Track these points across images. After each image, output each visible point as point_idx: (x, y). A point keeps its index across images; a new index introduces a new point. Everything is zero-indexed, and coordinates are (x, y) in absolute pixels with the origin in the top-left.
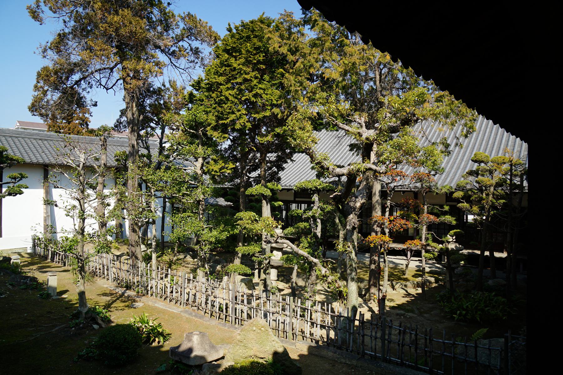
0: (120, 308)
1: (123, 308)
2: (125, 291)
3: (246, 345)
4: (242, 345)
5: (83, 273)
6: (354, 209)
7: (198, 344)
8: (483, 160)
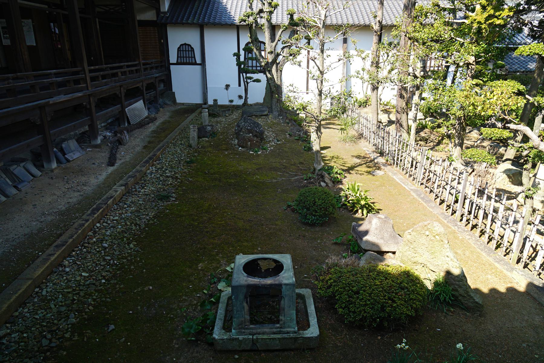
0: (360, 172)
1: (363, 173)
2: (378, 157)
3: (416, 249)
4: (412, 247)
5: (319, 133)
7: (376, 229)
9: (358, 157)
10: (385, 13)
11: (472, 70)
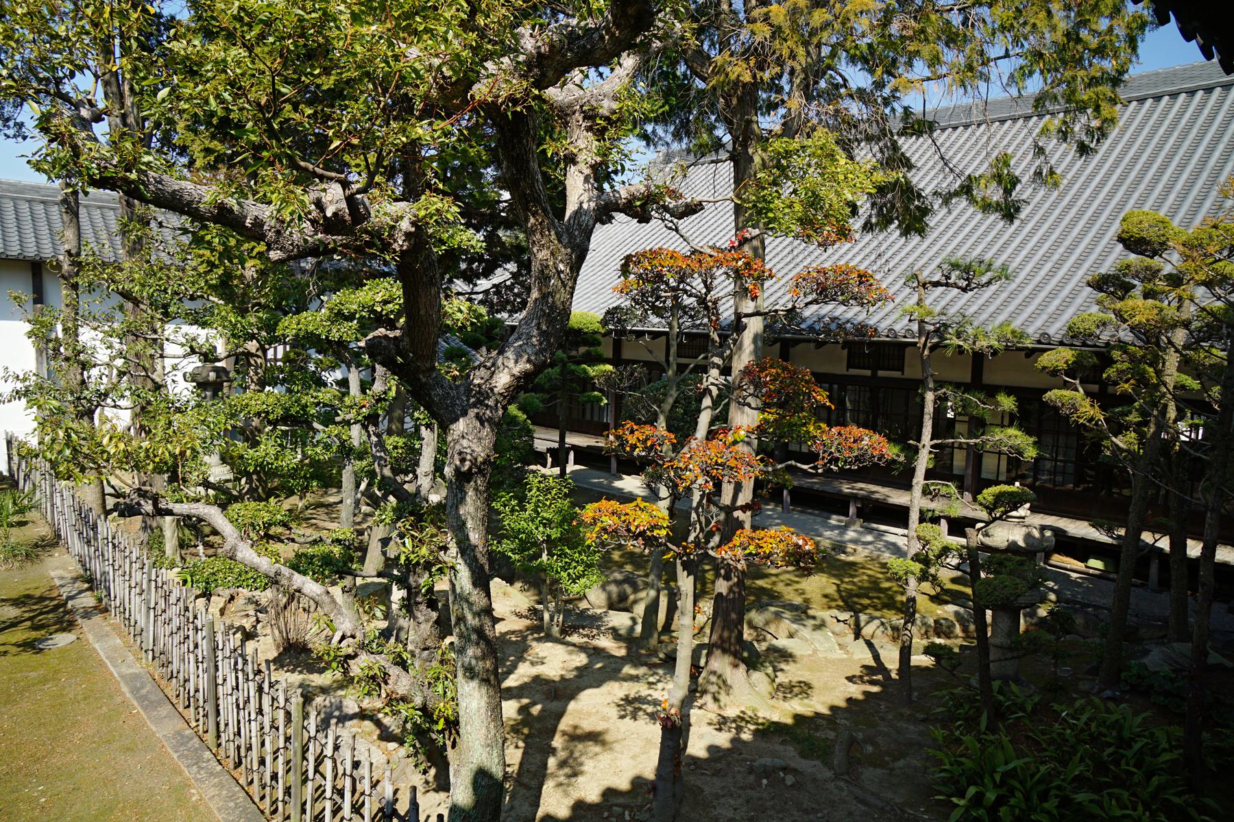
6: (482, 396)
8: (1144, 234)
9: (16, 602)
10: (993, 288)
11: (257, 367)
